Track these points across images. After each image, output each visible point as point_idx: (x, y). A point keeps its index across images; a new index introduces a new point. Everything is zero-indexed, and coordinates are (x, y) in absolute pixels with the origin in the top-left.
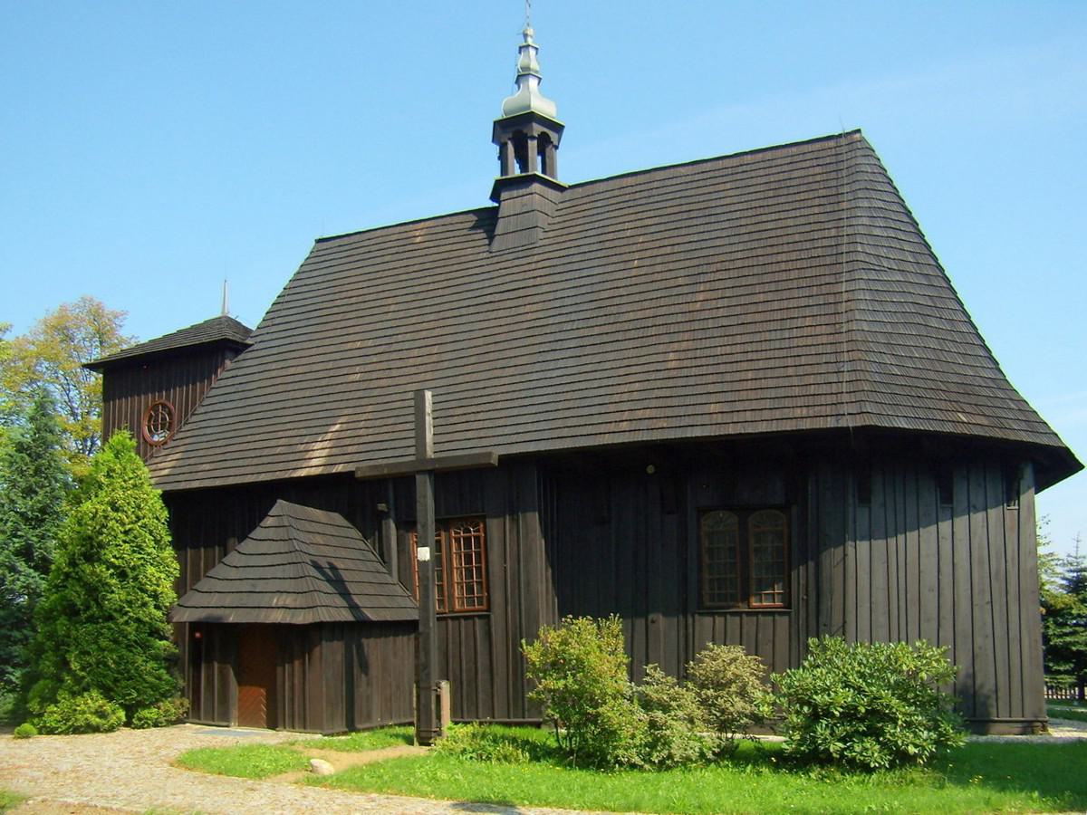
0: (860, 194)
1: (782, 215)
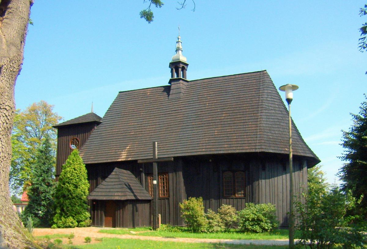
0: (265, 89)
1: (245, 93)
